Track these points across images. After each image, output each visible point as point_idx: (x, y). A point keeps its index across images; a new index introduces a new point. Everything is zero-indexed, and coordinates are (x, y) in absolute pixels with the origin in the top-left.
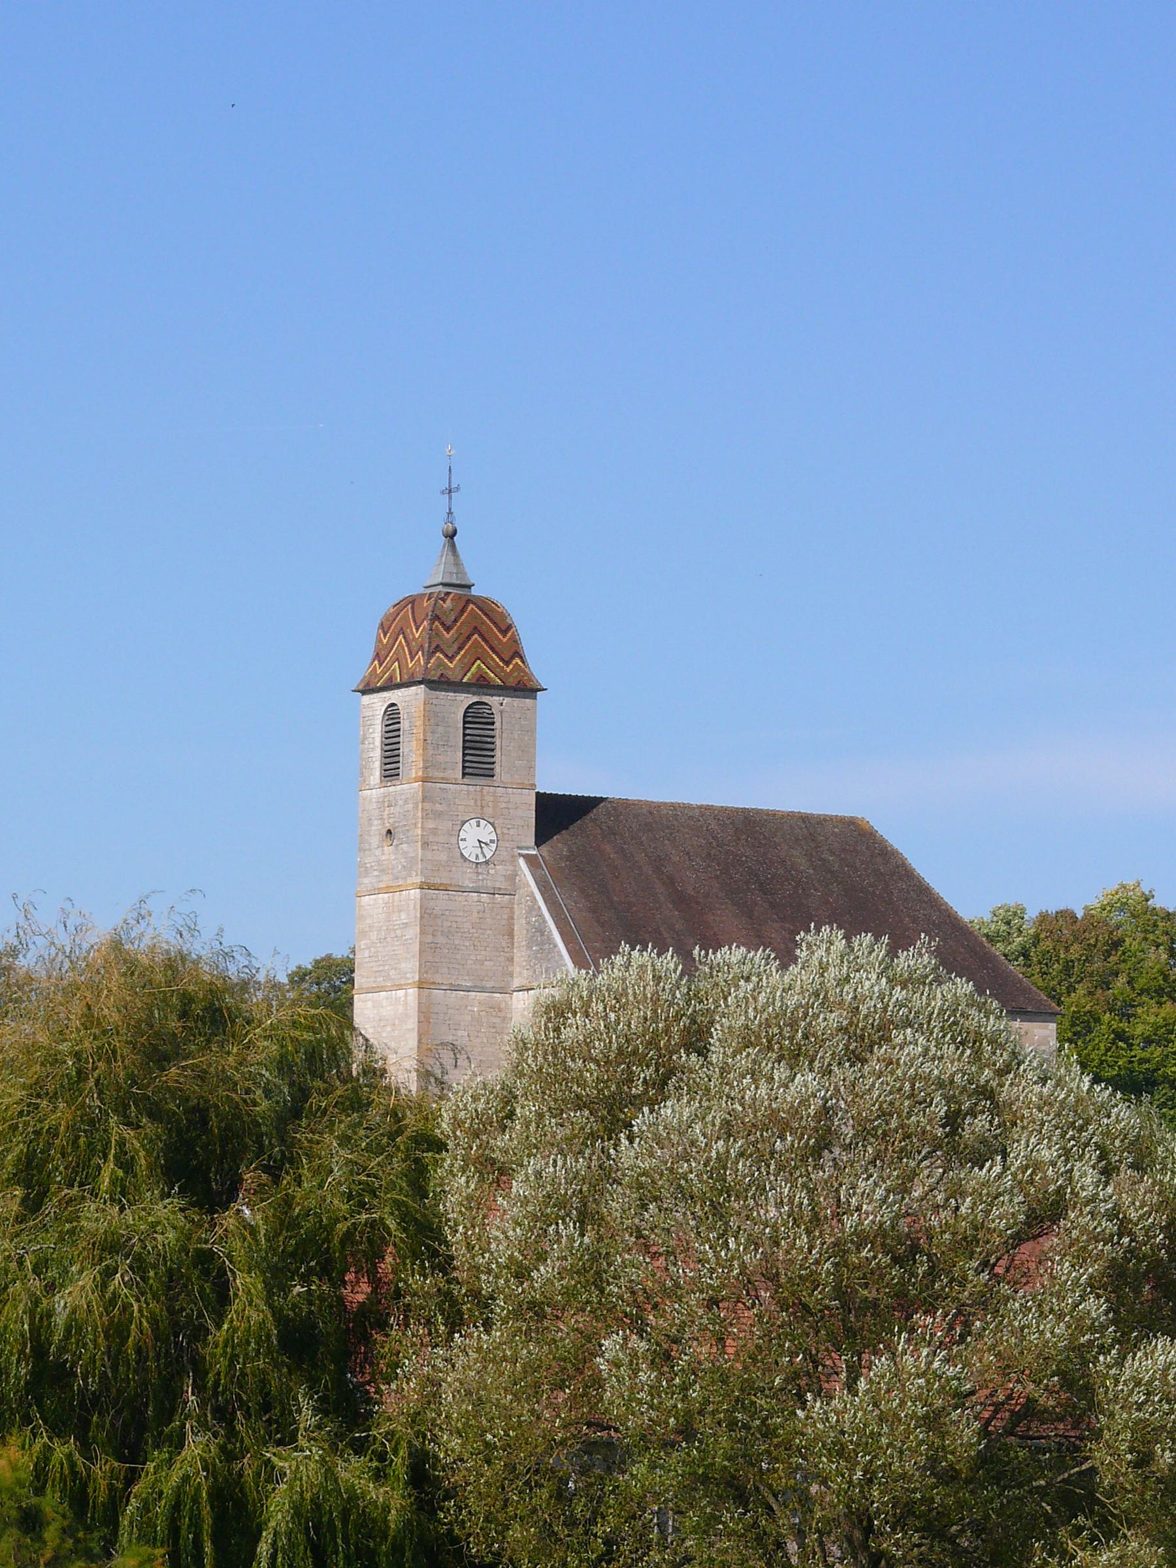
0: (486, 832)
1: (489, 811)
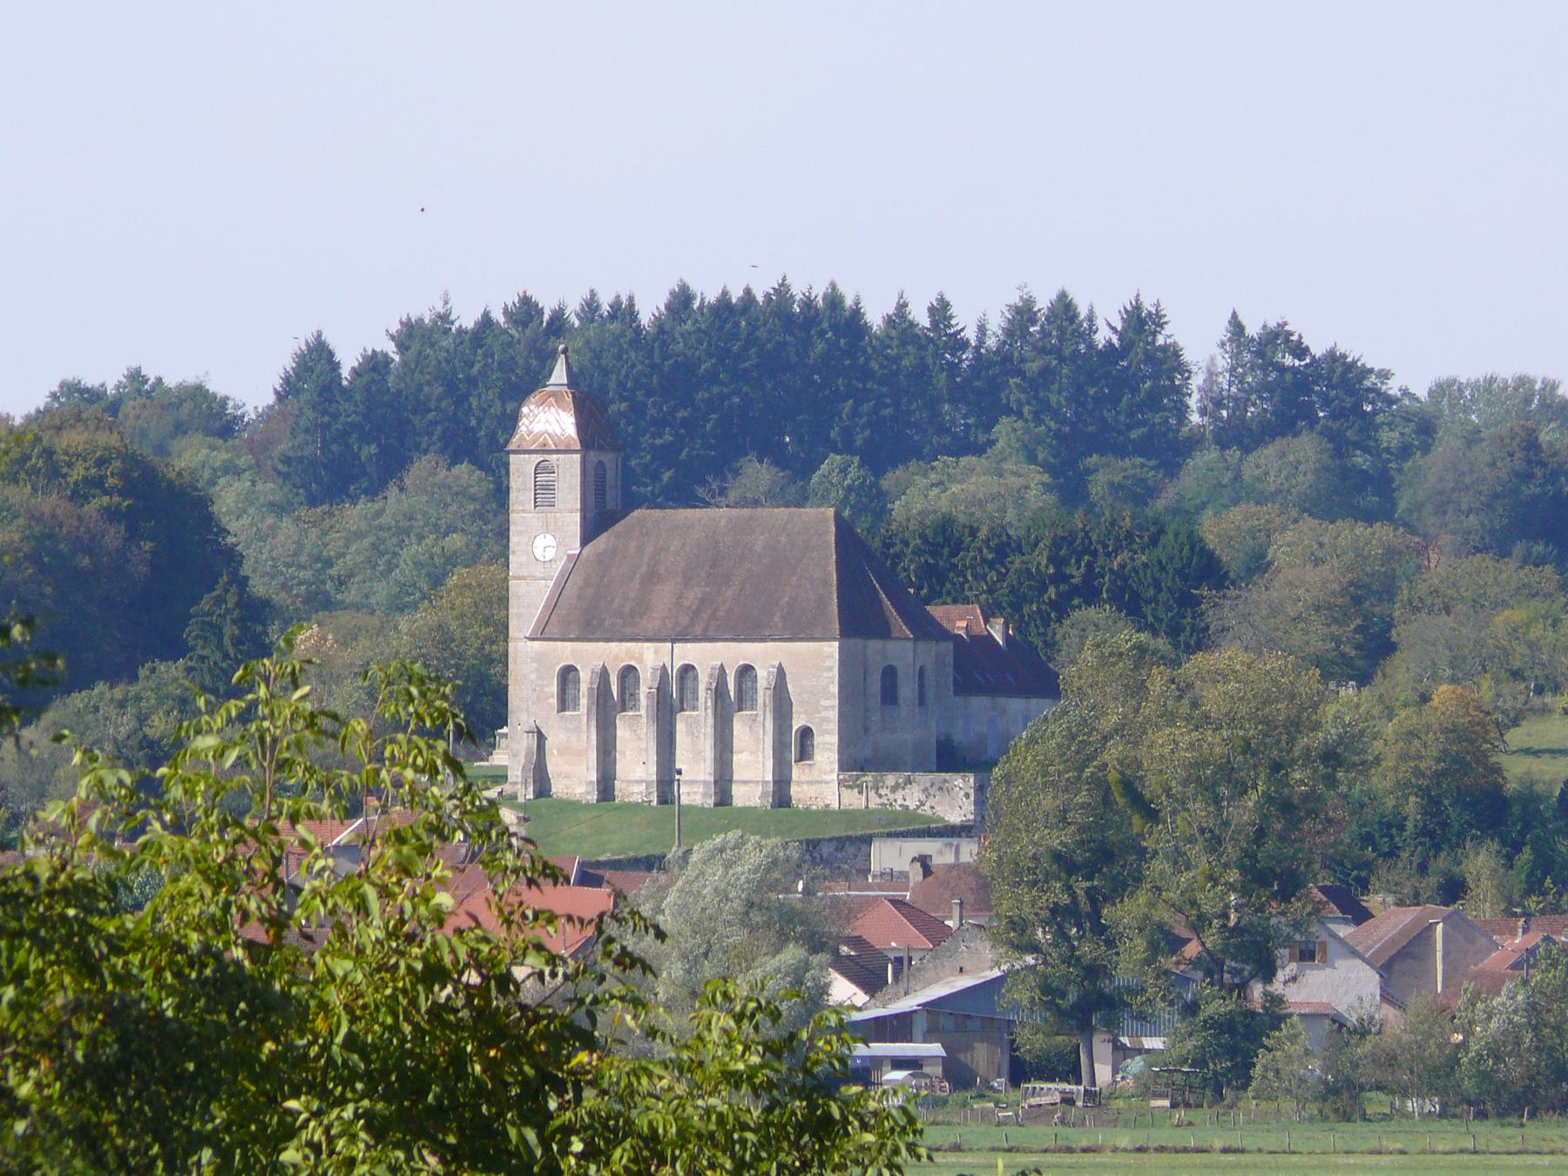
0: (550, 540)
1: (551, 528)
